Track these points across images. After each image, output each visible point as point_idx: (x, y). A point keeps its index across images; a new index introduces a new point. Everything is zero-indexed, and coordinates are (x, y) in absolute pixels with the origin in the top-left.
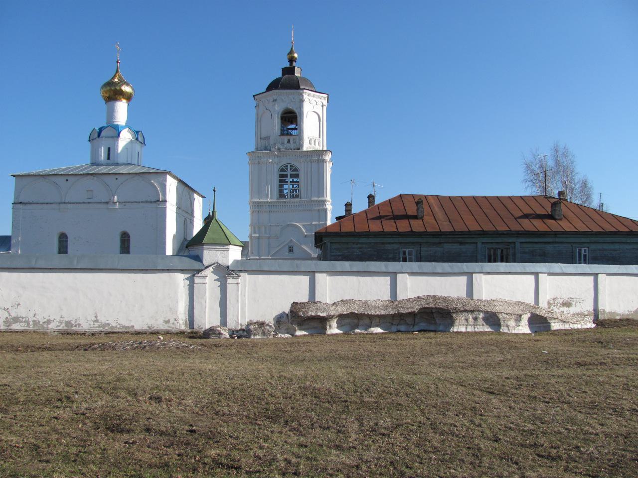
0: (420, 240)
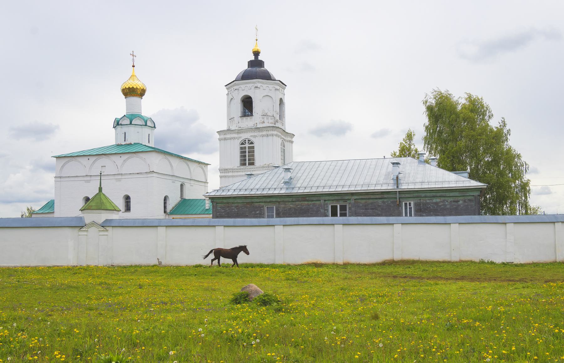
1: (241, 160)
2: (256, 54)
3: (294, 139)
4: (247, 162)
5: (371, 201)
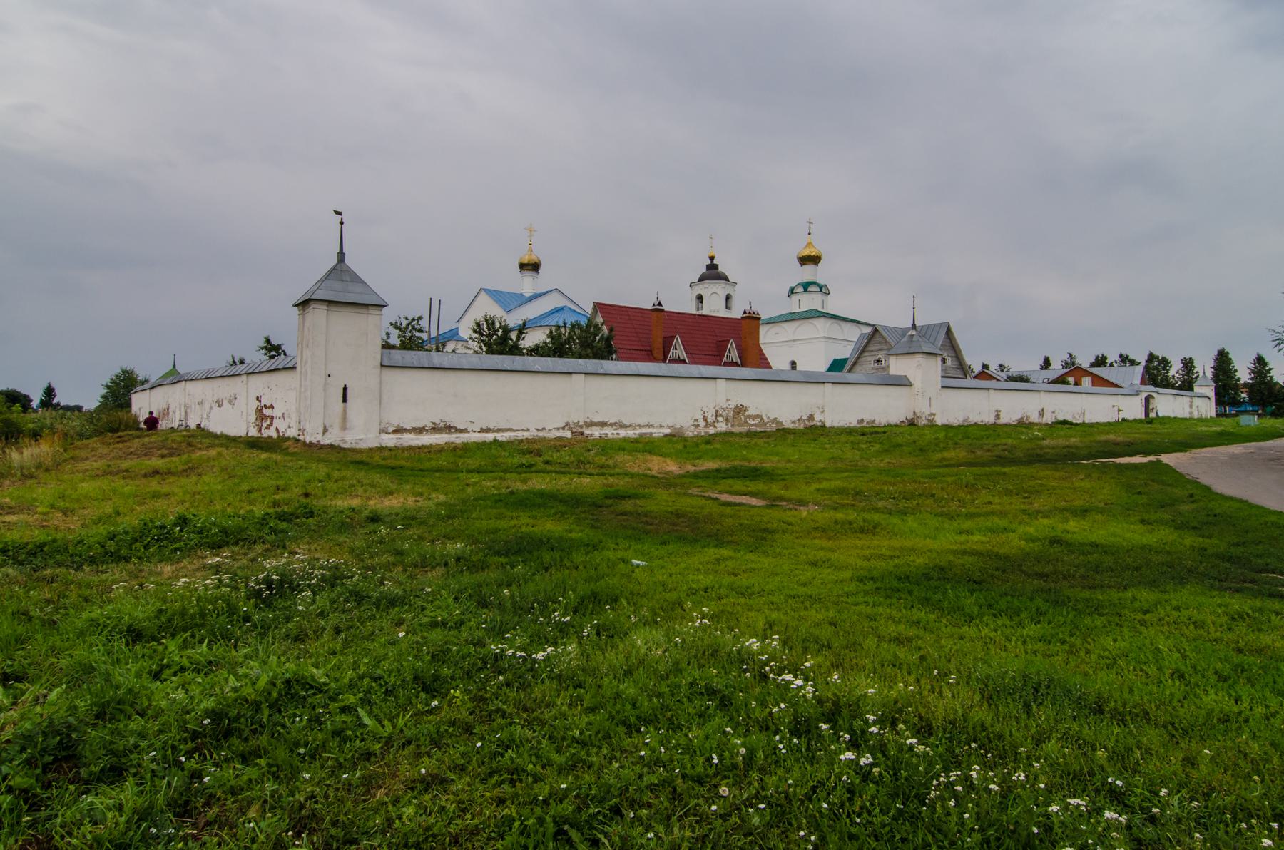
2: (712, 258)
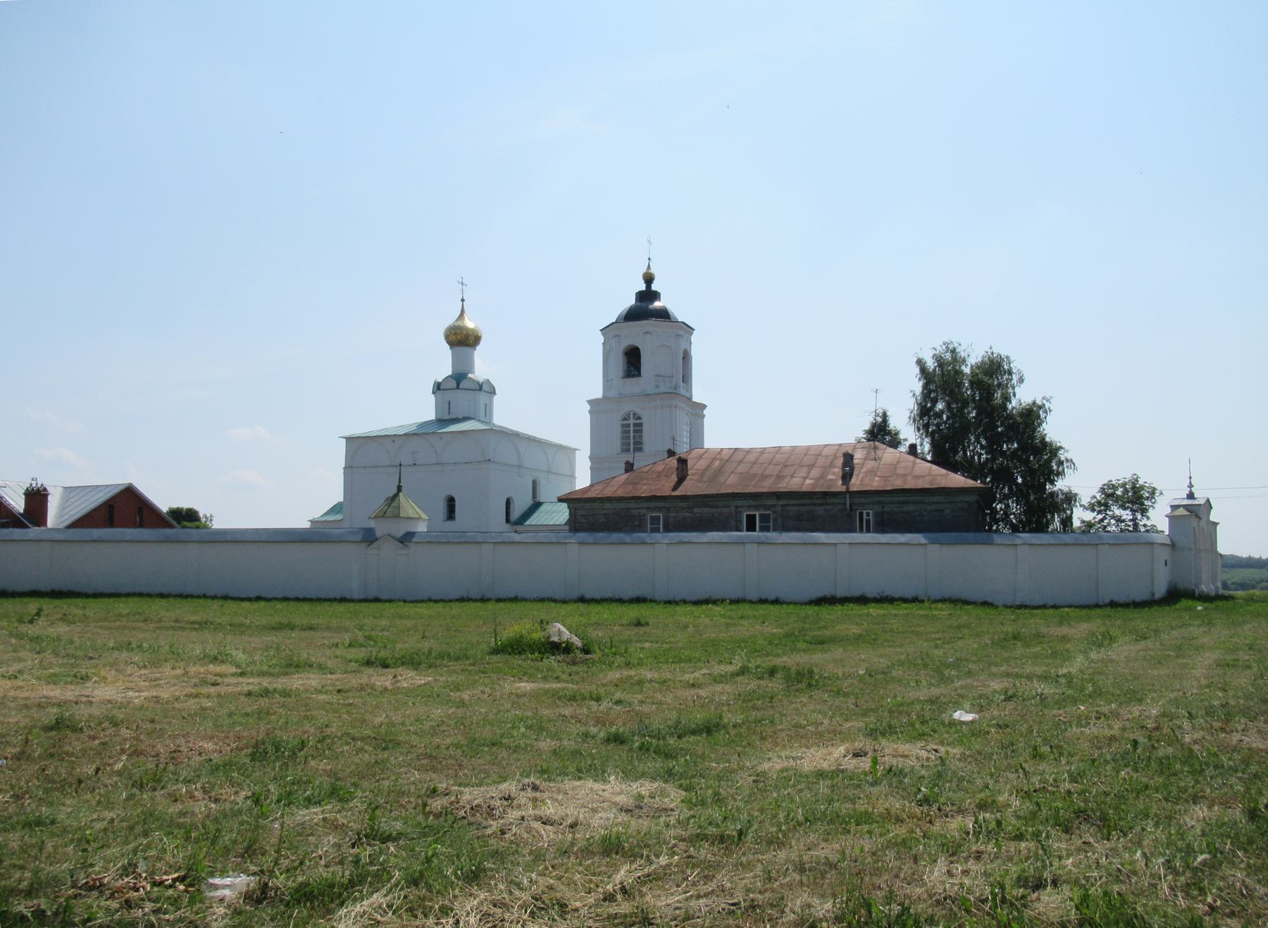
0: (666, 504)
1: (623, 444)
2: (649, 279)
3: (705, 412)
4: (632, 447)
5: (804, 509)
